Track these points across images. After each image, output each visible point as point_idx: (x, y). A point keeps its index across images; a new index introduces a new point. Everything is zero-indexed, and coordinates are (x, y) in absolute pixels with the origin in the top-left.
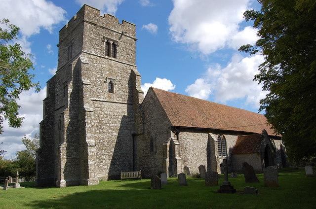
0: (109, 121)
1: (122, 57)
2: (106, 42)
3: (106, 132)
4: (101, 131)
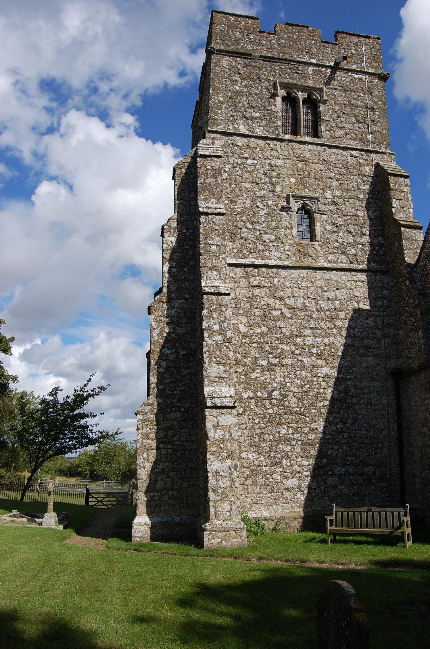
0: (301, 328)
1: (340, 133)
2: (284, 98)
3: (292, 365)
4: (274, 361)
